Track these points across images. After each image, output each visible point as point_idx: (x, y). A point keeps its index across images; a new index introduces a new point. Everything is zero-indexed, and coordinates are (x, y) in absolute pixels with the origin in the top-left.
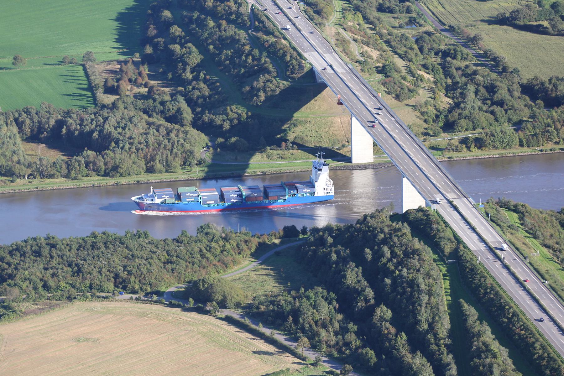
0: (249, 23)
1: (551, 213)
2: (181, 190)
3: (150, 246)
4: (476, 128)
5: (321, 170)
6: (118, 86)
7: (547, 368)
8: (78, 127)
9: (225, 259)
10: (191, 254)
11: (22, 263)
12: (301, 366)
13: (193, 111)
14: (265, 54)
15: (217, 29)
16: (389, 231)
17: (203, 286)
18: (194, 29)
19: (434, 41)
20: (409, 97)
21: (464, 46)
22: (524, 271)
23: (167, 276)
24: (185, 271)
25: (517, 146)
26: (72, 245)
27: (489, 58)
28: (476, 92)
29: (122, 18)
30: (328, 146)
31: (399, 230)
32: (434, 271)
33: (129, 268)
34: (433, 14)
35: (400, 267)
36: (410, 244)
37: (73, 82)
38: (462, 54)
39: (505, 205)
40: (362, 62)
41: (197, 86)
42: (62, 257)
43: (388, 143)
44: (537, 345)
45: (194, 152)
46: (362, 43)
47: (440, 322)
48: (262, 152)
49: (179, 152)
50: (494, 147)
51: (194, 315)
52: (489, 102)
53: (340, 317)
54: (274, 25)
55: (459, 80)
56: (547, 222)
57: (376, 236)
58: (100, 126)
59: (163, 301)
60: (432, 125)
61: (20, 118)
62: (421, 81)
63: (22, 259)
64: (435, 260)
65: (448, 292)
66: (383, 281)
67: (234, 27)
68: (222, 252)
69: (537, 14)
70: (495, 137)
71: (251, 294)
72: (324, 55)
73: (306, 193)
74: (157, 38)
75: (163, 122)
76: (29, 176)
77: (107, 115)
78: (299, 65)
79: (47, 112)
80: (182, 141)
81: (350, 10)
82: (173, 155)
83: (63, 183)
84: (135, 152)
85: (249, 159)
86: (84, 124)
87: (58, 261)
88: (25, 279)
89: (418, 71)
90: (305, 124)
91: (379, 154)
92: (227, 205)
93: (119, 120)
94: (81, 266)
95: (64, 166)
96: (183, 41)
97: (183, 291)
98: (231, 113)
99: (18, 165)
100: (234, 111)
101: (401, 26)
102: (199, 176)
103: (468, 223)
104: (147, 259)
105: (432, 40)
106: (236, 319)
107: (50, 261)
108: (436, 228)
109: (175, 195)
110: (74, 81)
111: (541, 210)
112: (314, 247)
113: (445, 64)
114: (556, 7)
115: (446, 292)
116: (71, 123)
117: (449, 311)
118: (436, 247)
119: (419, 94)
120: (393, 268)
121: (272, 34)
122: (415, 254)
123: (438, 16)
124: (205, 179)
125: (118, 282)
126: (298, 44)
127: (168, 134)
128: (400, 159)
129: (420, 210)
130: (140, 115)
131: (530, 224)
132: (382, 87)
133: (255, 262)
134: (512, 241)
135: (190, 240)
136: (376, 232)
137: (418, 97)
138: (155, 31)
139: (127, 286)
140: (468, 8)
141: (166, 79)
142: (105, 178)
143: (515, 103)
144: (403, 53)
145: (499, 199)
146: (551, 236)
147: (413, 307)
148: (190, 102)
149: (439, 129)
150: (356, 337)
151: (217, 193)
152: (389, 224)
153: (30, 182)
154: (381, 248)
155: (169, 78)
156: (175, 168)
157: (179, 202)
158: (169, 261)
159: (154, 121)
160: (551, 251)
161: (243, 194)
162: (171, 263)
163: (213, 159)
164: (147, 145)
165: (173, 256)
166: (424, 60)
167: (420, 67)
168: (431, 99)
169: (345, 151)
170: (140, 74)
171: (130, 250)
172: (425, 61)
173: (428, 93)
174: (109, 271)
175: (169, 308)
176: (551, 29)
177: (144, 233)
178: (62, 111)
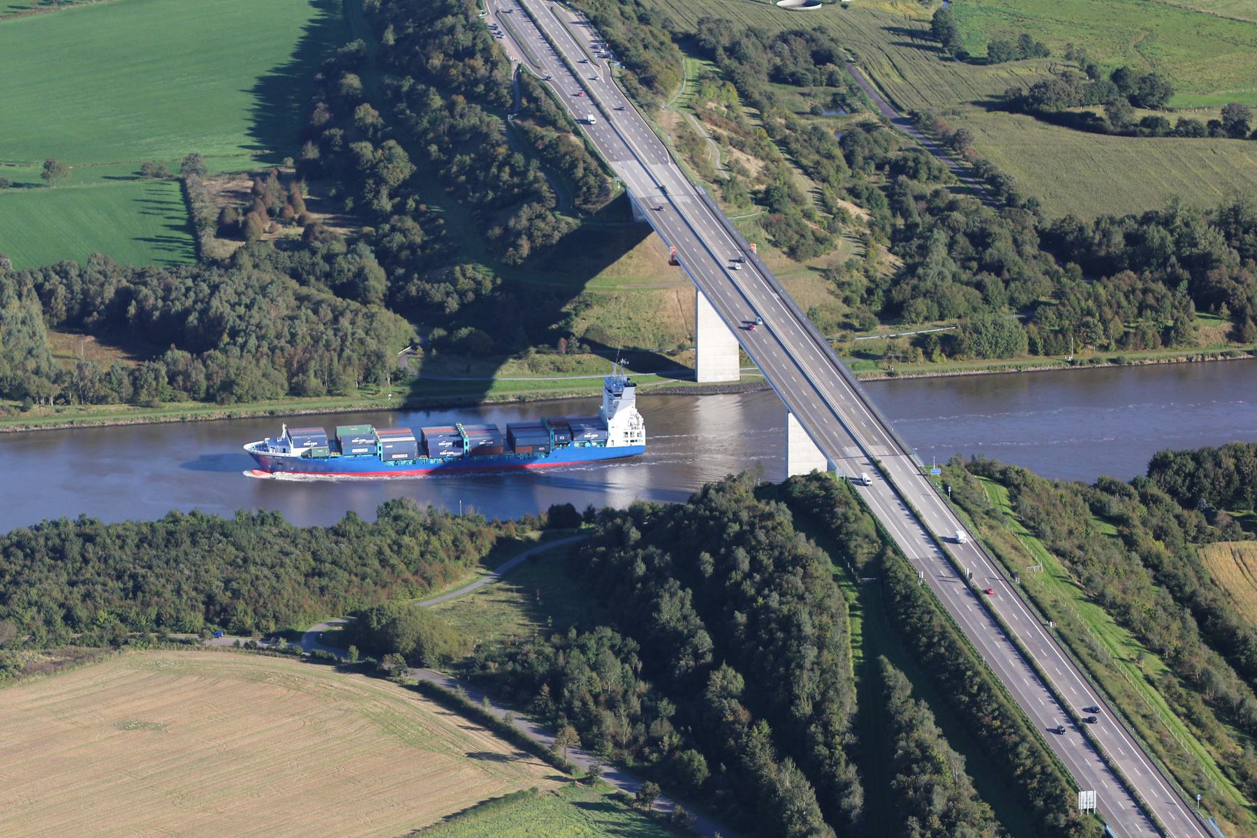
0: (511, 101)
1: (1076, 487)
2: (342, 431)
3: (280, 541)
4: (946, 316)
5: (620, 395)
6: (245, 223)
7: (1039, 796)
8: (160, 303)
9: (428, 568)
10: (360, 558)
11: (27, 571)
12: (559, 784)
13: (389, 273)
17: (379, 622)
18: (403, 112)
21: (934, 153)
22: (1009, 601)
23: (310, 602)
24: (346, 592)
25: (1025, 353)
26: (127, 536)
27: (982, 177)
28: (951, 246)
30: (650, 346)
31: (770, 516)
33: (234, 585)
34: (880, 88)
36: (789, 546)
37: (158, 214)
38: (929, 169)
40: (725, 183)
41: (399, 224)
42: (106, 561)
43: (762, 344)
44: (1023, 750)
47: (837, 700)
48: (520, 358)
49: (355, 356)
50: (979, 354)
51: (358, 679)
52: (974, 265)
53: (643, 687)
54: (558, 107)
55: (918, 220)
56: (1065, 505)
57: (723, 527)
58: (202, 301)
59: (300, 650)
60: (858, 308)
61: (47, 283)
62: (844, 220)
63: (28, 563)
64: (836, 578)
65: (858, 642)
66: (732, 617)
68: (422, 554)
70: (981, 333)
71: (473, 639)
72: (652, 167)
73: (589, 441)
74: (330, 128)
75: (328, 295)
76: (56, 399)
78: (600, 187)
79: (100, 273)
80: (360, 333)
81: (713, 78)
82: (342, 362)
84: (267, 355)
85: (493, 370)
86: (172, 297)
88: (30, 604)
89: (839, 200)
90: (607, 303)
92: (432, 461)
93: (241, 289)
94: (140, 579)
95: (126, 381)
97: (340, 631)
98: (461, 279)
99: (35, 378)
101: (814, 112)
103: (905, 504)
104: (273, 567)
105: (872, 140)
106: (439, 689)
107: (81, 568)
108: (843, 514)
110: (160, 212)
111: (1057, 481)
112: (603, 549)
113: (893, 189)
114: (1122, 78)
115: (853, 641)
117: (857, 679)
119: (836, 248)
120: (753, 592)
121: (553, 124)
123: (890, 92)
124: (406, 409)
125: (212, 612)
126: (601, 145)
127: (336, 320)
128: (783, 376)
129: (814, 477)
130: (284, 279)
131: (1029, 509)
132: (763, 232)
134: (991, 541)
137: (833, 253)
138: (327, 116)
140: (950, 77)
141: (341, 210)
142: (207, 405)
143: (1025, 267)
144: (811, 165)
145: (973, 458)
146: (1071, 532)
147: (787, 669)
148: (385, 257)
150: (672, 728)
152: (751, 504)
153: (58, 411)
154: (733, 552)
155: (348, 209)
156: (345, 385)
157: (338, 455)
160: (1067, 562)
161: (465, 441)
162: (320, 575)
163: (421, 371)
164: (293, 339)
165: (324, 562)
167: (844, 193)
168: (859, 257)
169: (684, 357)
170: (290, 199)
172: (855, 181)
174: (196, 589)
175: (309, 664)
176: (1108, 122)
177: (272, 514)
178: (130, 271)
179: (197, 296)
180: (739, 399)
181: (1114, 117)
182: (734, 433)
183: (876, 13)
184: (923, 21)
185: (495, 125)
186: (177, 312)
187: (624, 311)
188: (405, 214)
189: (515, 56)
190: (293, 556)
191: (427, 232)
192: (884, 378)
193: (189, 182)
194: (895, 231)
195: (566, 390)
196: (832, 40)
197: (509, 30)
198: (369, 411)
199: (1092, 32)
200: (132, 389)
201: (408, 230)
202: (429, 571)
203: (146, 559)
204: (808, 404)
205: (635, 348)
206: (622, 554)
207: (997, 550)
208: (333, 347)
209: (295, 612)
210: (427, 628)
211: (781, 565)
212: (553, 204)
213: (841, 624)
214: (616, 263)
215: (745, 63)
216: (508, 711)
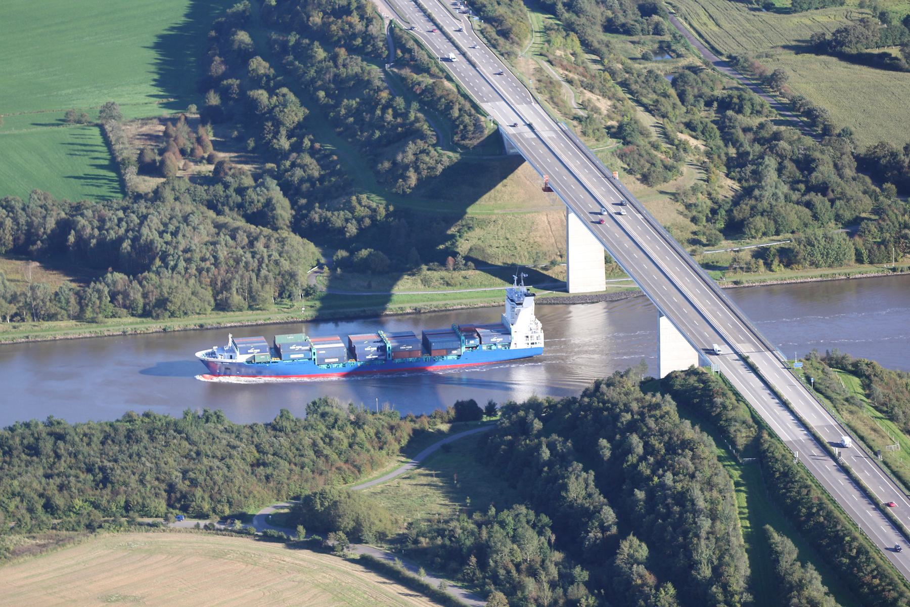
0: (387, 52)
2: (280, 340)
3: (226, 436)
5: (521, 304)
6: (162, 162)
8: (96, 232)
9: (357, 457)
10: (297, 449)
13: (293, 204)
15: (331, 64)
16: (639, 408)
17: (322, 505)
18: (291, 63)
19: (703, 82)
20: (665, 178)
21: (755, 91)
22: (875, 475)
23: (258, 489)
24: (288, 479)
25: (852, 263)
26: (93, 435)
27: (798, 110)
28: (780, 170)
31: (657, 406)
32: (719, 478)
33: (191, 475)
34: (700, 35)
35: (661, 470)
36: (677, 431)
37: (84, 155)
38: (752, 105)
40: (584, 119)
42: (75, 456)
43: (633, 258)
45: (298, 275)
46: (582, 86)
47: (732, 564)
48: (413, 275)
49: (271, 275)
50: (812, 264)
51: (306, 555)
52: (802, 187)
53: (558, 556)
54: (430, 56)
55: (749, 149)
57: (617, 417)
58: (133, 230)
59: (253, 530)
60: (705, 226)
63: (7, 459)
64: (720, 459)
65: (744, 514)
66: (632, 494)
67: (360, 58)
68: (351, 446)
70: (814, 246)
71: (403, 519)
72: (518, 106)
73: (495, 344)
75: (241, 223)
77: (145, 211)
78: (475, 125)
79: (41, 207)
80: (275, 256)
82: (260, 281)
83: (71, 328)
84: (195, 275)
85: (391, 286)
86: (106, 227)
88: (14, 495)
89: (678, 133)
91: (615, 278)
93: (166, 220)
94: (109, 471)
95: (73, 300)
98: (358, 207)
100: (363, 204)
101: (645, 57)
102: (306, 316)
103: (775, 394)
105: (699, 81)
106: (379, 561)
107: (54, 463)
109: (271, 348)
110: (85, 153)
112: (510, 437)
113: (724, 122)
115: (740, 513)
116: (84, 226)
117: (747, 546)
118: (722, 436)
119: (682, 174)
120: (648, 472)
123: (709, 39)
126: (472, 88)
127: (251, 244)
128: (654, 284)
129: (691, 372)
131: (881, 396)
132: (619, 161)
134: (853, 424)
135: (296, 425)
136: (618, 410)
137: (680, 179)
138: (223, 67)
139: (189, 506)
140: (761, 26)
141: (245, 150)
142: (144, 320)
144: (651, 103)
145: (827, 352)
147: (685, 538)
148: (288, 189)
149: (718, 233)
150: (587, 591)
151: (342, 345)
152: (638, 396)
153: (14, 327)
155: (250, 148)
157: (278, 360)
158: (261, 461)
162: (265, 464)
163: (329, 287)
164: (216, 264)
165: (267, 453)
166: (688, 115)
167: (682, 127)
168: (702, 182)
170: (199, 140)
174: (157, 479)
176: (904, 61)
179: (128, 226)
185: (375, 73)
186: (111, 240)
188: (303, 151)
189: (386, 13)
190: (239, 449)
191: (323, 167)
192: (731, 286)
193: (108, 128)
194: (729, 159)
198: (286, 323)
200: (78, 308)
201: (306, 165)
202: (359, 460)
203: (111, 454)
204: (679, 308)
205: (513, 265)
206: (528, 441)
207: (859, 432)
210: (364, 509)
211: (671, 449)
213: (729, 499)
214: (492, 191)
215: (581, 16)
216: (441, 580)
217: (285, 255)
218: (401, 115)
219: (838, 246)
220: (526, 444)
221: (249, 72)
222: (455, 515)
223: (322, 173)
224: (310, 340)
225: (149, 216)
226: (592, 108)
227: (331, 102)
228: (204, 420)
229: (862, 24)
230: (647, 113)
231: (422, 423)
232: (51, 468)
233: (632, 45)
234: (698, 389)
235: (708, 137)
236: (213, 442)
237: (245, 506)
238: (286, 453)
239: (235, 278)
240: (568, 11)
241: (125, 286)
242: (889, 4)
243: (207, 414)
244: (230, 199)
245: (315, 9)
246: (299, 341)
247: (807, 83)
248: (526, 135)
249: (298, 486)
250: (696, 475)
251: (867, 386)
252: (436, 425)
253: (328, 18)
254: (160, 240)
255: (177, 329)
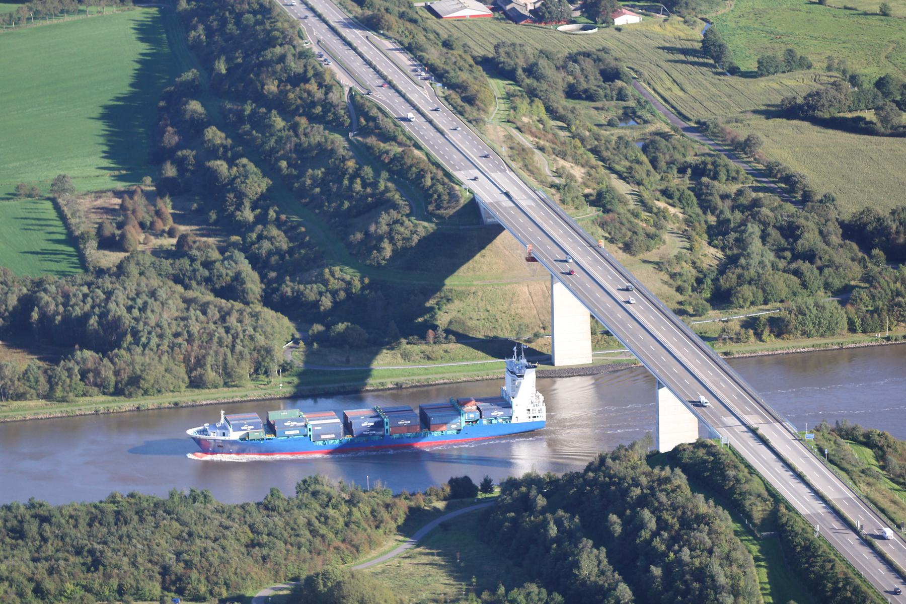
0: (349, 121)
2: (273, 416)
3: (217, 516)
4: (770, 300)
5: (522, 376)
6: (123, 236)
8: (61, 309)
10: (292, 529)
13: (263, 277)
14: (385, 174)
15: (291, 133)
16: (649, 482)
17: (325, 585)
18: (249, 133)
19: (674, 148)
20: (648, 247)
21: (730, 157)
23: (255, 570)
24: (285, 559)
25: (845, 332)
27: (775, 176)
28: (764, 237)
29: (111, 115)
30: (507, 334)
31: (667, 480)
32: (738, 552)
34: (666, 100)
35: (676, 545)
36: (690, 506)
37: (39, 230)
38: (728, 171)
39: (847, 434)
40: (562, 187)
42: (62, 539)
43: (627, 329)
45: (274, 350)
46: (554, 153)
48: (392, 349)
49: (246, 351)
50: (804, 333)
52: (788, 254)
57: (625, 492)
60: (691, 296)
64: (736, 533)
65: (766, 589)
66: (648, 570)
67: (322, 127)
69: (852, 99)
70: (805, 315)
72: (492, 174)
73: (496, 418)
74: (181, 149)
75: (210, 297)
77: (110, 286)
78: (449, 194)
80: (250, 331)
83: (41, 408)
84: (167, 352)
85: (370, 361)
86: (71, 303)
87: (55, 545)
91: (601, 350)
93: (132, 295)
94: (98, 554)
95: (42, 379)
96: (229, 154)
100: (337, 276)
101: (611, 124)
102: (284, 393)
103: (789, 466)
104: (216, 540)
105: (671, 147)
107: (41, 546)
108: (734, 477)
109: (264, 425)
110: (40, 228)
112: (513, 514)
113: (701, 189)
114: (884, 85)
115: (762, 589)
116: (48, 302)
118: (738, 510)
119: (664, 243)
120: (663, 548)
121: (394, 139)
122: (702, 522)
126: (442, 156)
127: (223, 319)
128: (652, 355)
131: (897, 468)
132: (600, 230)
133: (404, 541)
134: (872, 496)
135: (289, 504)
136: (626, 485)
137: (663, 247)
138: (176, 138)
139: (184, 589)
140: (727, 89)
141: (206, 222)
142: (116, 398)
144: (624, 170)
145: (837, 423)
148: (256, 262)
149: (705, 302)
151: (338, 420)
155: (212, 221)
158: (255, 542)
159: (195, 296)
162: (260, 545)
163: (306, 363)
165: (261, 534)
166: (663, 182)
167: (658, 194)
169: (540, 344)
170: (158, 213)
171: (183, 523)
173: (679, 239)
174: (150, 561)
176: (879, 125)
177: (203, 493)
179: (93, 301)
180: (593, 381)
181: (885, 120)
182: (591, 413)
183: (649, 35)
184: (692, 40)
185: (339, 142)
186: (77, 316)
187: (482, 304)
191: (291, 239)
193: (60, 200)
195: (438, 376)
196: (616, 59)
197: (335, 59)
199: (844, 45)
200: (47, 387)
203: (99, 536)
204: (681, 380)
205: (495, 337)
206: (532, 518)
207: (879, 504)
208: (225, 344)
209: (243, 579)
212: (407, 210)
215: (542, 81)
217: (259, 330)
218: (370, 185)
219: (830, 315)
220: (530, 520)
221: (206, 142)
222: (461, 594)
223: (291, 245)
224: (304, 416)
225: (116, 291)
226: (567, 176)
227: (295, 172)
228: (191, 500)
229: (834, 87)
230: (621, 181)
231: (417, 501)
232: (38, 550)
233: (596, 112)
234: (708, 462)
235: (685, 204)
236: (205, 523)
237: (243, 588)
238: (281, 533)
239: (209, 354)
240: (528, 77)
241: (95, 363)
242: (857, 67)
243: (194, 493)
244: (197, 273)
245: (270, 77)
246: (293, 417)
247: (781, 148)
248: (504, 204)
249: (296, 567)
250: (714, 550)
251: (881, 457)
252: (431, 503)
253: (285, 86)
254: (128, 316)
255: (151, 407)
